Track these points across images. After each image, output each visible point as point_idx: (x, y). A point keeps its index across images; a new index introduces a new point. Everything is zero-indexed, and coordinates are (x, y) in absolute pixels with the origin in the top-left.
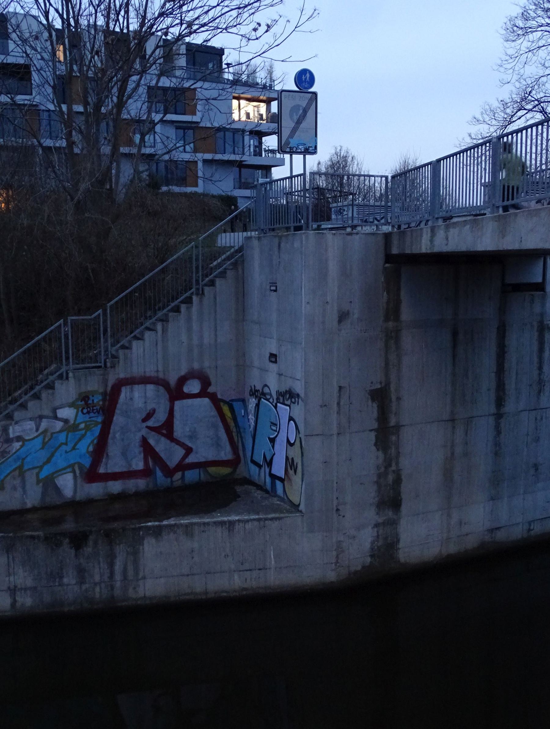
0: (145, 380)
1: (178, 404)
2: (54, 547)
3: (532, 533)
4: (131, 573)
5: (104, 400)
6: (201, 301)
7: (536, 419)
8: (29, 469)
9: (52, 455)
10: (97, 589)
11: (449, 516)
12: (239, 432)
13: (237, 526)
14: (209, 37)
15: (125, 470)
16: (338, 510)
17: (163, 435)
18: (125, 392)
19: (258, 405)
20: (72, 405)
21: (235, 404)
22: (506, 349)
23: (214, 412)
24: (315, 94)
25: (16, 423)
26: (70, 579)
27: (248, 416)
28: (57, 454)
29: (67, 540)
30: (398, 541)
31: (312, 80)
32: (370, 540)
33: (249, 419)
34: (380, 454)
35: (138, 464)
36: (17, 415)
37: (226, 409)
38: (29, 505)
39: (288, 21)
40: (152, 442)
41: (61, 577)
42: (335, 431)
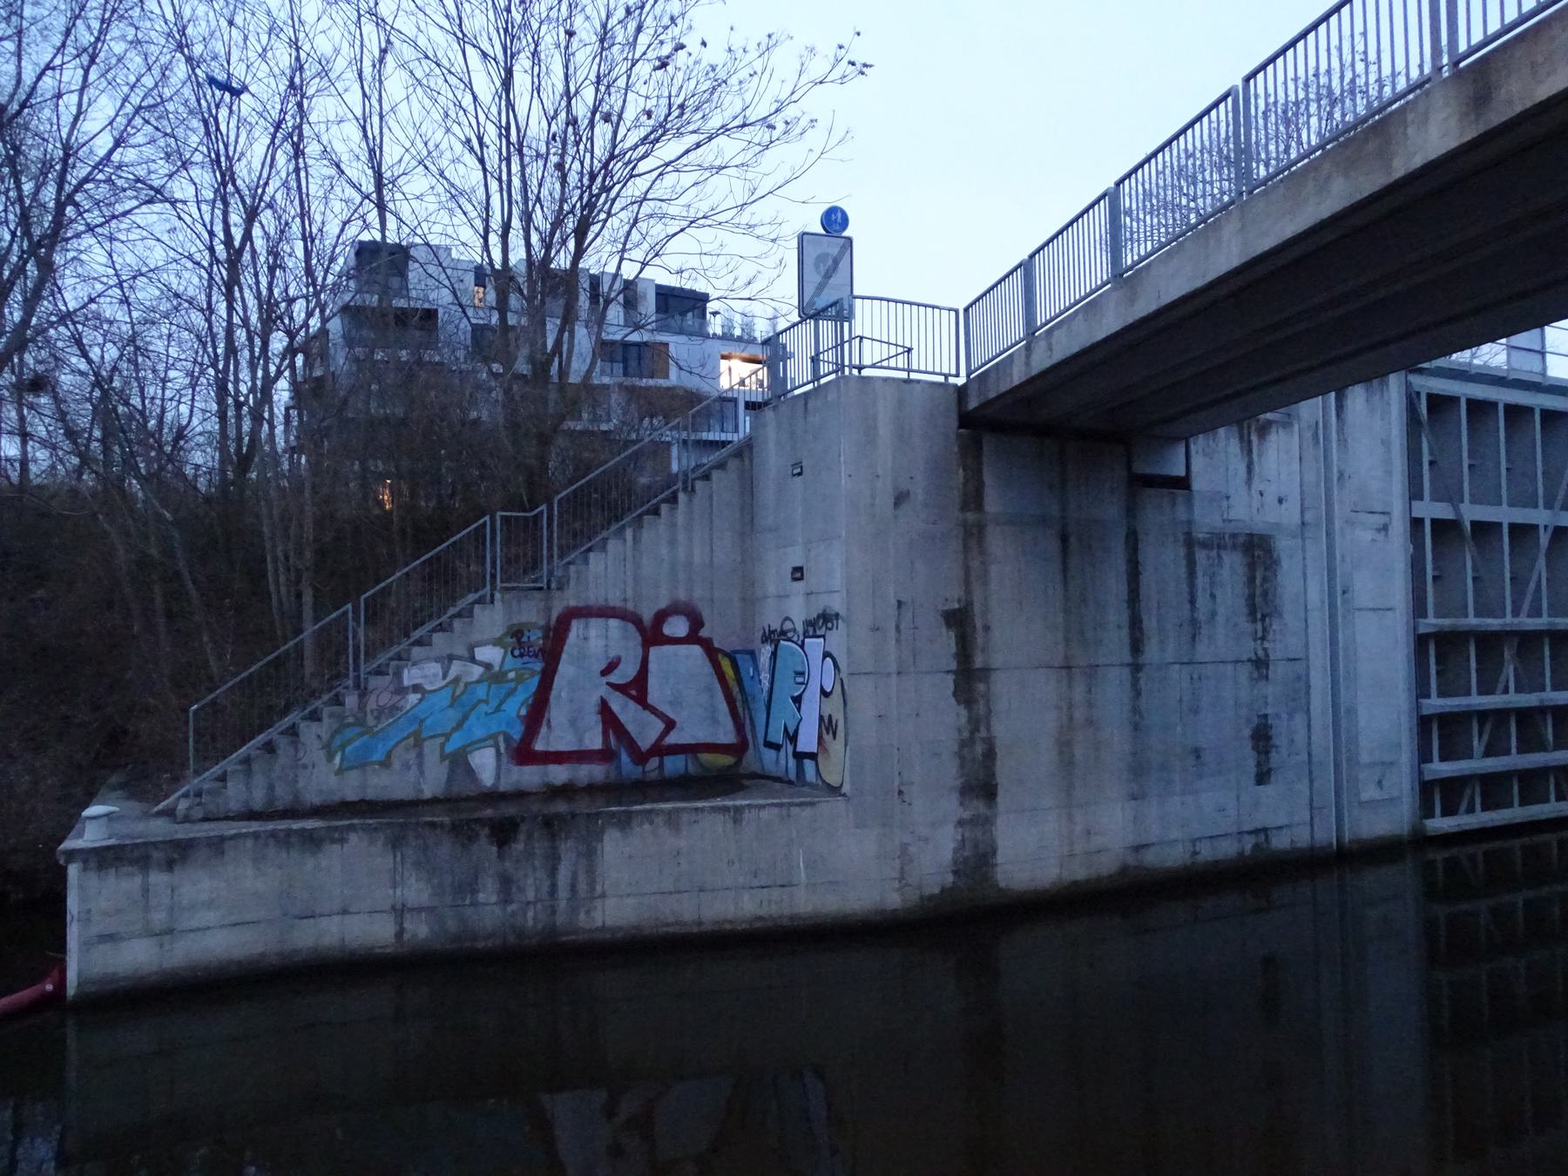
0: (606, 612)
1: (654, 652)
2: (466, 842)
3: (1200, 858)
4: (582, 887)
5: (545, 637)
6: (690, 501)
7: (1192, 678)
8: (431, 737)
9: (465, 717)
10: (530, 914)
11: (1070, 818)
12: (745, 701)
13: (746, 815)
14: (702, 179)
15: (575, 748)
16: (900, 792)
17: (632, 698)
18: (576, 627)
19: (774, 654)
20: (497, 642)
21: (738, 656)
22: (1140, 568)
23: (708, 668)
24: (850, 240)
25: (414, 664)
26: (488, 894)
27: (759, 675)
28: (472, 718)
29: (486, 831)
30: (994, 852)
31: (845, 222)
32: (952, 845)
33: (760, 681)
34: (964, 712)
35: (594, 741)
36: (417, 652)
37: (726, 665)
38: (427, 794)
39: (811, 150)
40: (615, 707)
41: (474, 892)
42: (893, 668)
